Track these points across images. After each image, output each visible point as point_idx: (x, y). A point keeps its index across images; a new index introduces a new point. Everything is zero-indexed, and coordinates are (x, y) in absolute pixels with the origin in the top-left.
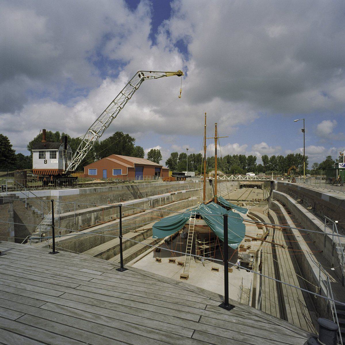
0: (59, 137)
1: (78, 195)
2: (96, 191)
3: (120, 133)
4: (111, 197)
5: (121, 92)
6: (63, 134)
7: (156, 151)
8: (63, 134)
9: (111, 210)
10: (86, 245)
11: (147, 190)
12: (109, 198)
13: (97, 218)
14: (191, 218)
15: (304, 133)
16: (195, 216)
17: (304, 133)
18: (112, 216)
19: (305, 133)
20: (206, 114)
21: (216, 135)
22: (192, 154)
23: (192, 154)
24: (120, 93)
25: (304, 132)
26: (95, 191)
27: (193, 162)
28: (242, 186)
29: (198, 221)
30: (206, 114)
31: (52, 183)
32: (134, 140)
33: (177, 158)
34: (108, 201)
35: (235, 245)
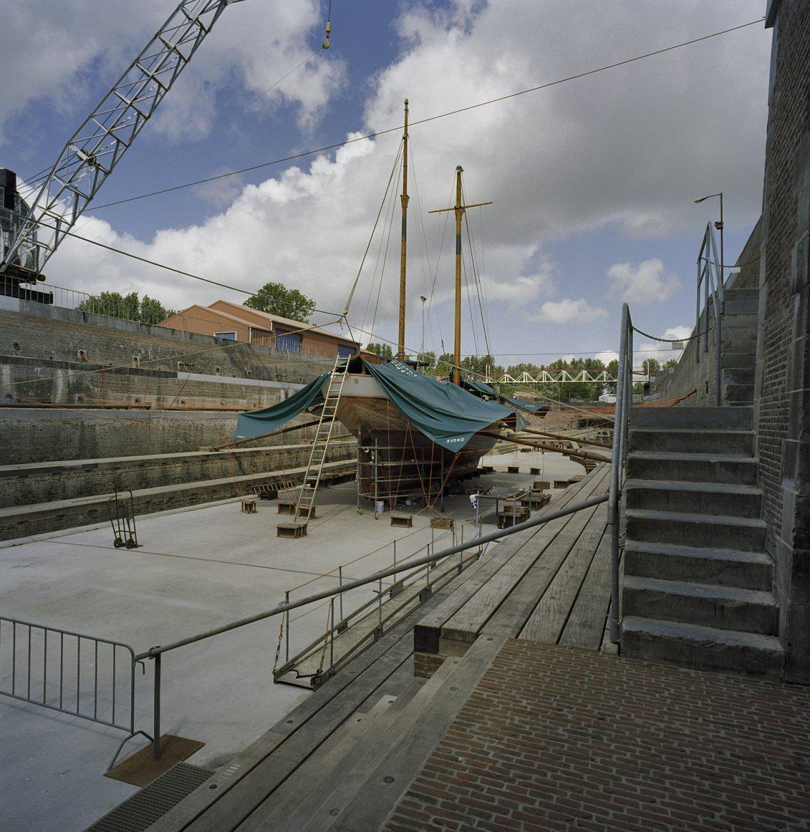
0: (135, 307)
1: (13, 313)
2: (90, 320)
3: (277, 287)
4: (147, 352)
5: (156, 35)
6: (146, 298)
7: (382, 350)
8: (146, 298)
9: (136, 378)
10: (15, 447)
11: (279, 366)
12: (140, 351)
13: (74, 388)
14: (336, 371)
15: (722, 232)
16: (347, 367)
17: (722, 232)
18: (140, 396)
19: (724, 229)
20: (406, 103)
21: (459, 199)
22: (470, 358)
23: (470, 358)
24: (155, 38)
25: (722, 228)
26: (82, 320)
27: (472, 378)
28: (585, 423)
29: (356, 381)
30: (406, 103)
31: (629, 821)
32: (313, 306)
33: (434, 366)
34: (136, 359)
35: (459, 440)
